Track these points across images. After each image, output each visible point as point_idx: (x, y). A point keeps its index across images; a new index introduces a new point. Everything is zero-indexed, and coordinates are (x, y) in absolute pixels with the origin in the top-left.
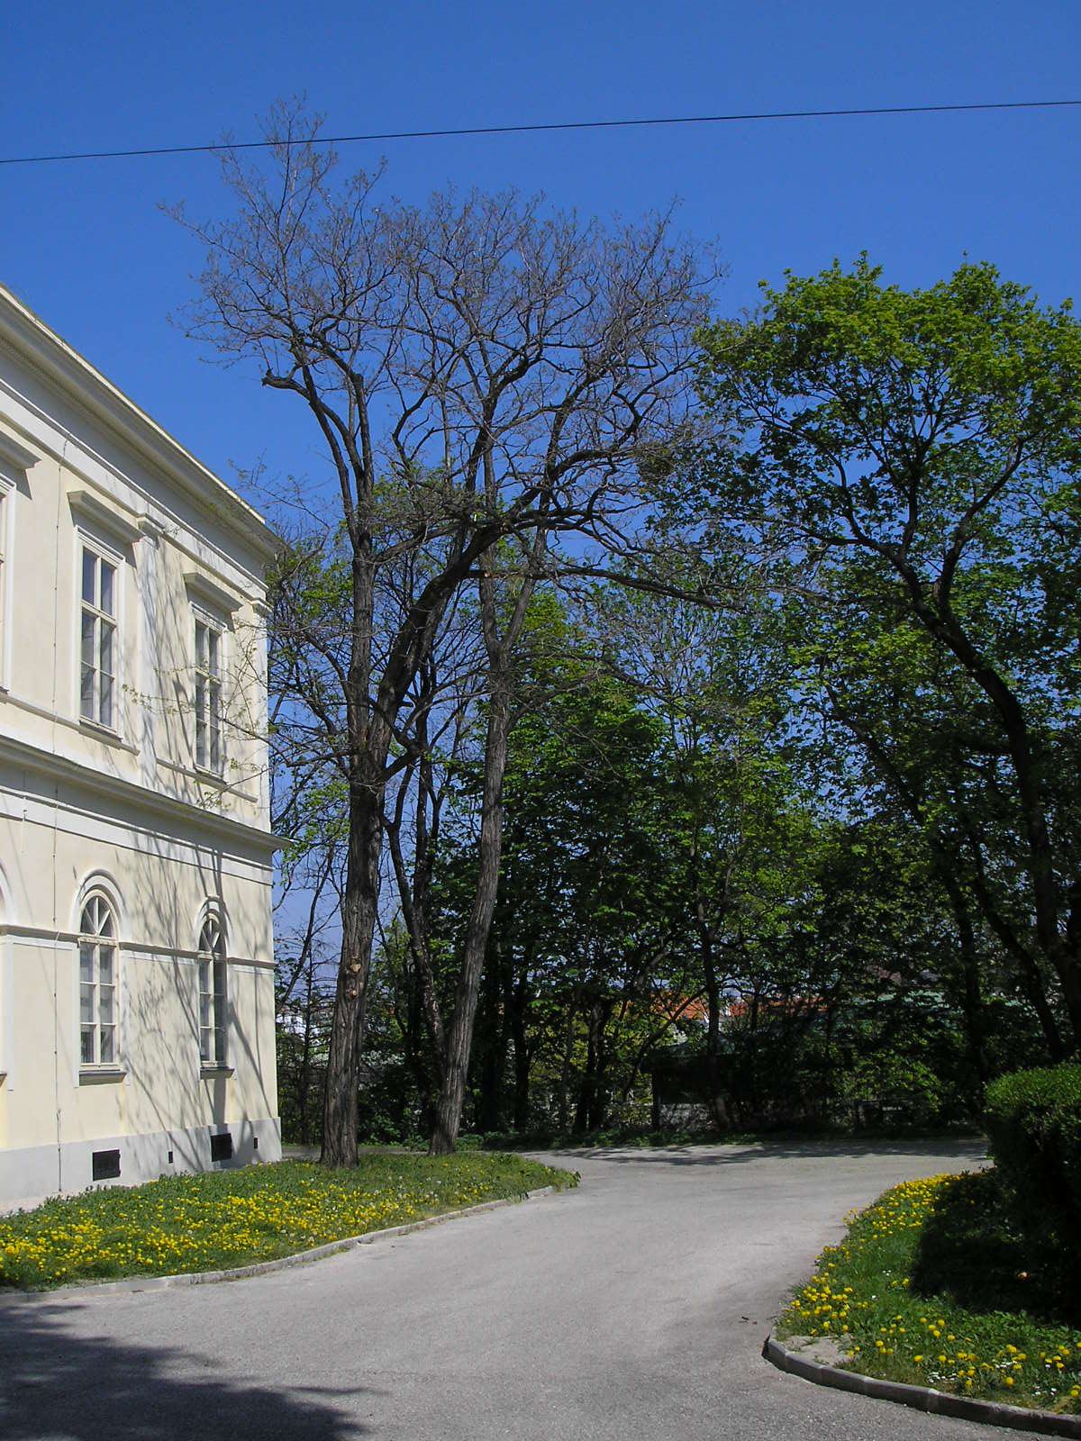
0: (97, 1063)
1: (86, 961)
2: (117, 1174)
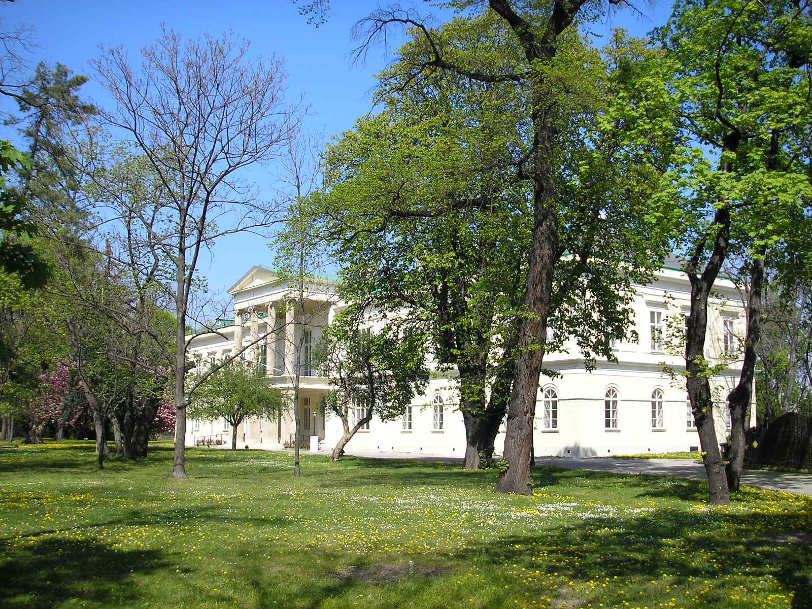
0: (658, 427)
1: (436, 410)
2: (309, 448)
